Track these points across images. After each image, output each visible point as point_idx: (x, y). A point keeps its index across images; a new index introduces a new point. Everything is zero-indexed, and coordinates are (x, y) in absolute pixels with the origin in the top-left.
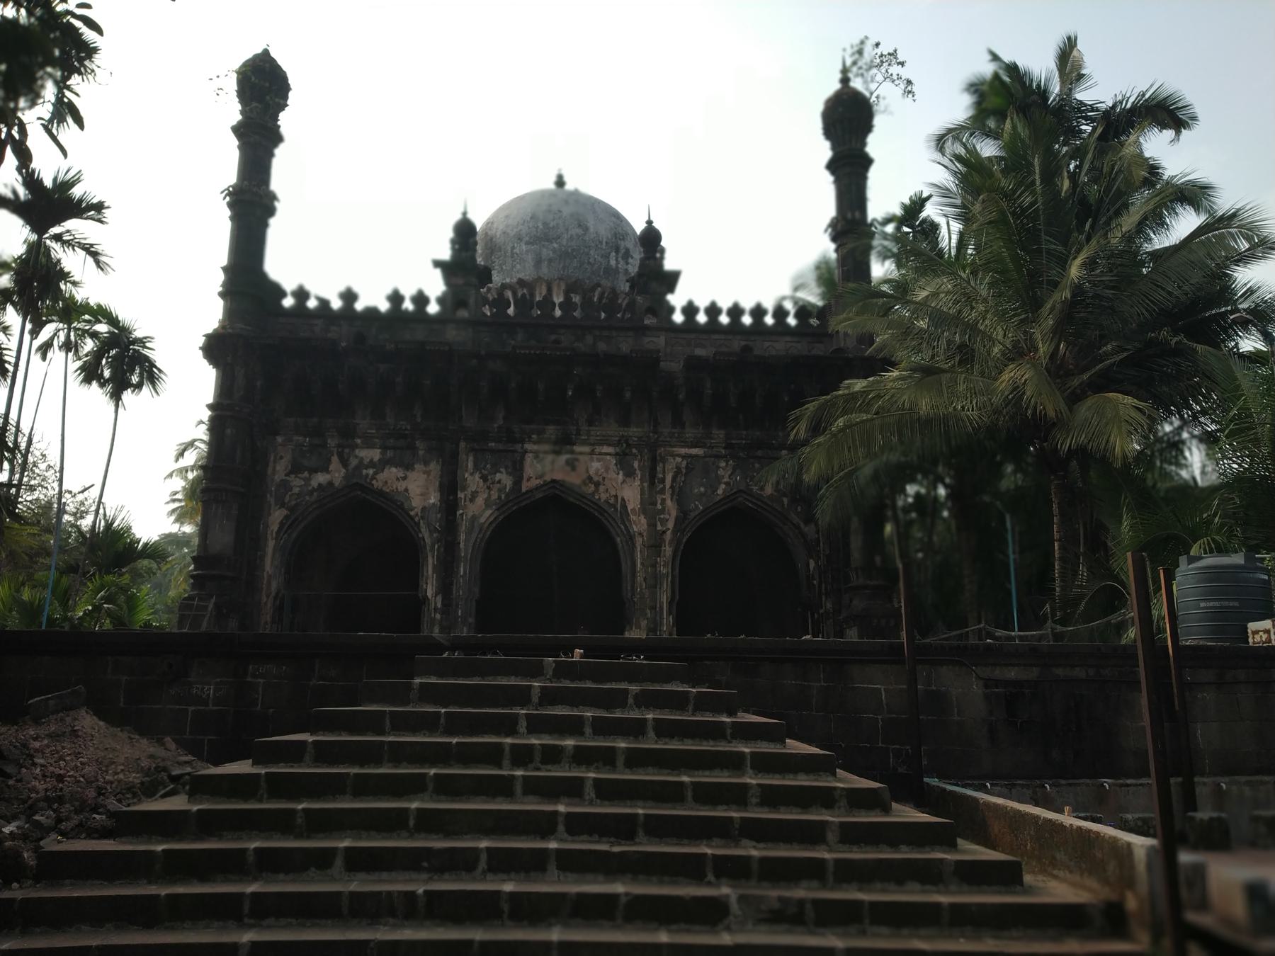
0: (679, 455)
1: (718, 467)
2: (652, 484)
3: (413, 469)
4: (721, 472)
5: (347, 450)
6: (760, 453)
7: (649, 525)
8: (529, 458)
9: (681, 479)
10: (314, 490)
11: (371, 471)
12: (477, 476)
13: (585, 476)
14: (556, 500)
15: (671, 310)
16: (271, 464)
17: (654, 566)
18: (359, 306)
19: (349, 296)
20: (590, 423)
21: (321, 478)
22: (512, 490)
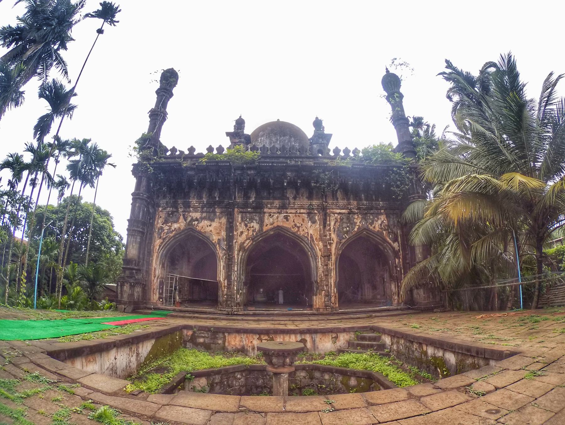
0: (336, 213)
1: (354, 218)
2: (325, 227)
3: (214, 221)
4: (355, 220)
5: (186, 213)
6: (372, 211)
7: (324, 246)
8: (266, 216)
9: (338, 224)
10: (173, 231)
11: (196, 223)
12: (243, 224)
13: (293, 224)
14: (279, 234)
15: (329, 150)
16: (157, 220)
17: (327, 265)
18: (195, 153)
19: (192, 149)
20: (295, 198)
21: (176, 226)
22: (259, 231)
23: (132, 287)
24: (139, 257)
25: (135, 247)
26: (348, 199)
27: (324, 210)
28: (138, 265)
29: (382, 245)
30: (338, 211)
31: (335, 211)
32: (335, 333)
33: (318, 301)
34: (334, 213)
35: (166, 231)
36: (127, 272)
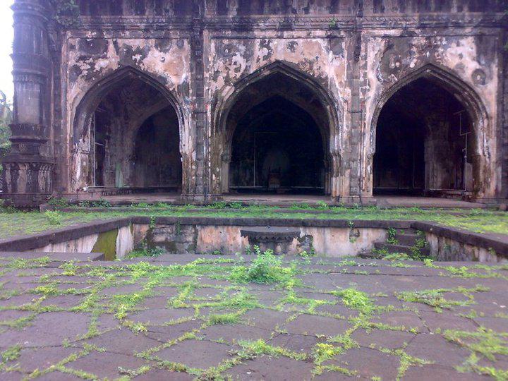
0: (379, 36)
11: (138, 57)
23: (34, 169)
24: (41, 119)
25: (32, 103)
26: (403, 9)
27: (355, 31)
28: (41, 133)
29: (460, 94)
30: (383, 32)
31: (376, 32)
32: (444, 338)
33: (340, 184)
34: (374, 37)
35: (85, 73)
36: (23, 147)
